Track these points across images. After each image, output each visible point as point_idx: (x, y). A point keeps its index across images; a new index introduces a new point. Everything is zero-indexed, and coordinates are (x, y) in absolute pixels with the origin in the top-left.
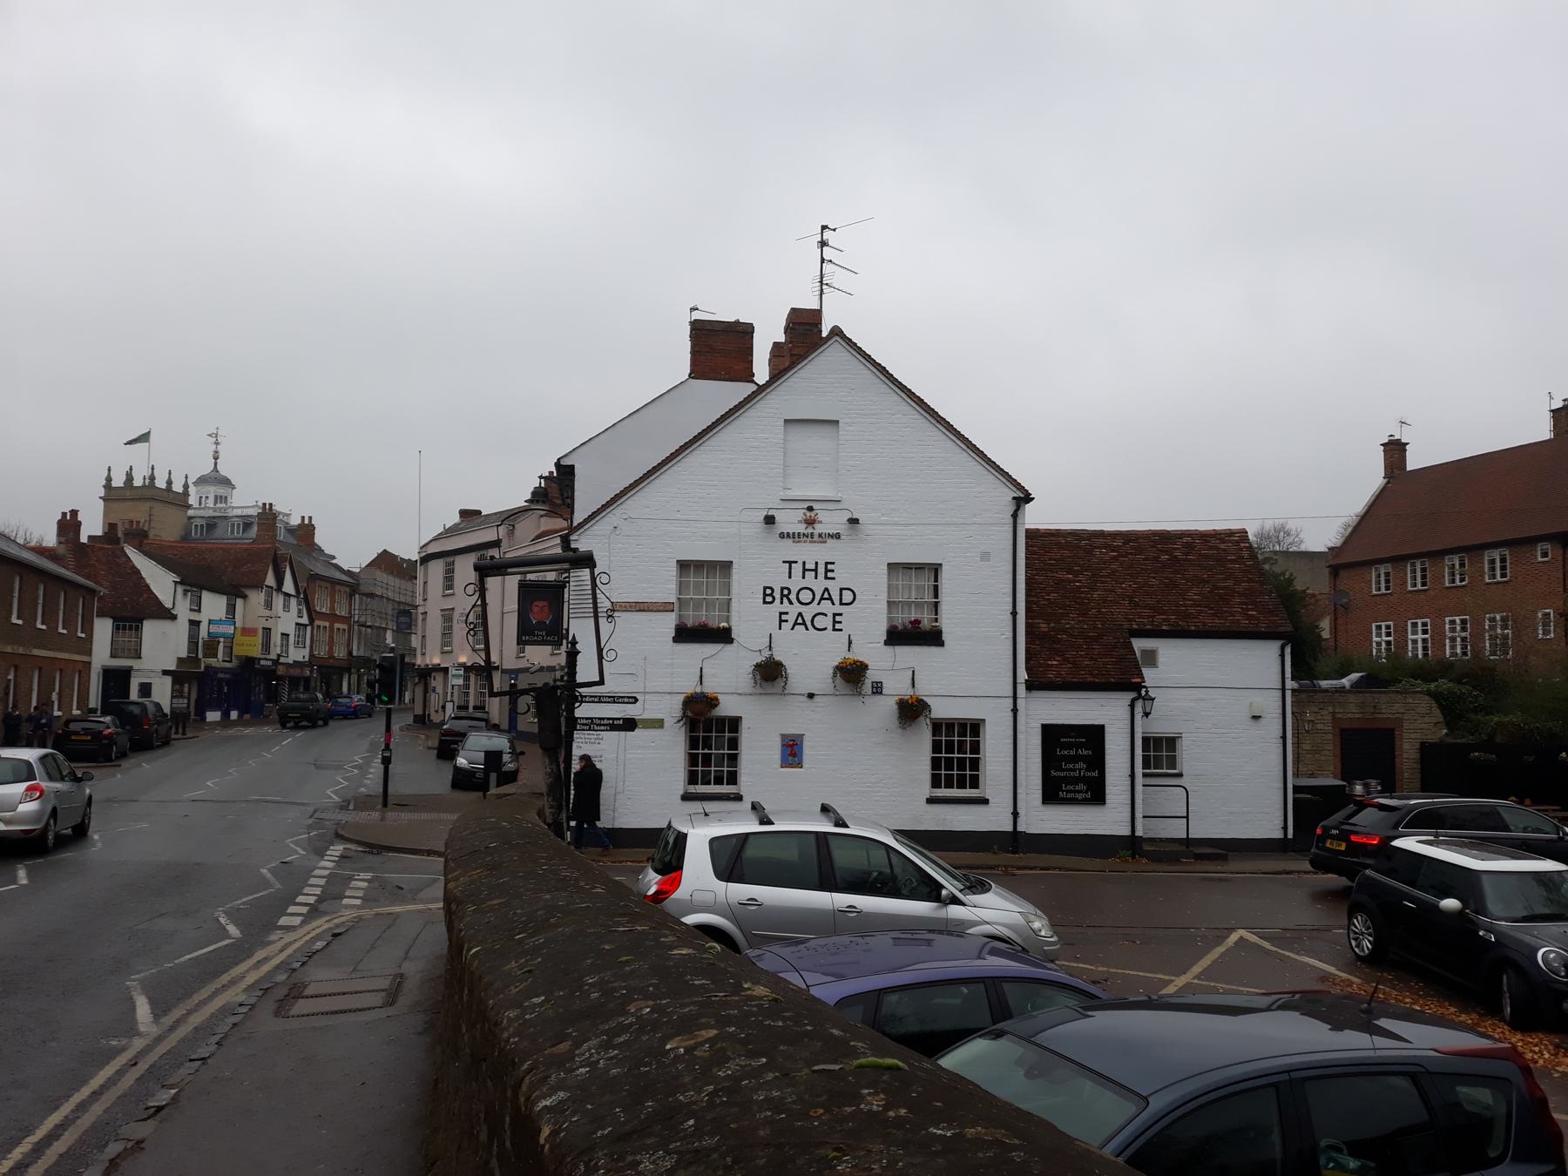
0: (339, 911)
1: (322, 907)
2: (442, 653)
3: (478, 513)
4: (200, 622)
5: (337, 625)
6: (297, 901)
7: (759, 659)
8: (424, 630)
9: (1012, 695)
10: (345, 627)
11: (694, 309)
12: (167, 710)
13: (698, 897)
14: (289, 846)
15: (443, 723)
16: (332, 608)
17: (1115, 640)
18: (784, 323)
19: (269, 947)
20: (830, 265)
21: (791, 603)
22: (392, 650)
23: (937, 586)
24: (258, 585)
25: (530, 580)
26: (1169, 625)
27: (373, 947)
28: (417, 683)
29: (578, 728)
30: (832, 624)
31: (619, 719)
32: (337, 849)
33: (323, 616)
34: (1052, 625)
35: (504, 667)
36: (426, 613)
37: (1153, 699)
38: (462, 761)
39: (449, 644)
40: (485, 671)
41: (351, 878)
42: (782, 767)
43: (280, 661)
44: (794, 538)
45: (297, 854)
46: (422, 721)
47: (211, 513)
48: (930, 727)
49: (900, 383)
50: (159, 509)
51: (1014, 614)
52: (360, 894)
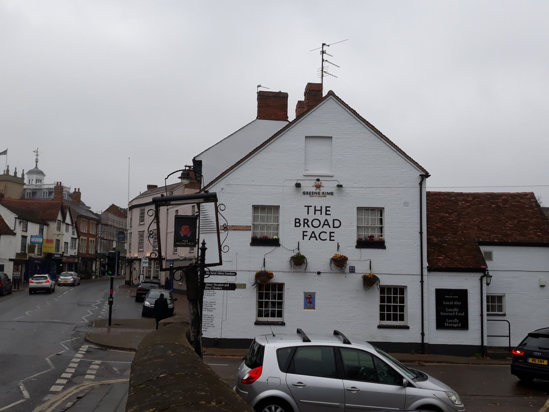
0: (83, 383)
1: (75, 380)
2: (139, 252)
3: (156, 186)
4: (27, 236)
5: (90, 239)
6: (62, 376)
7: (293, 254)
8: (130, 241)
9: (420, 274)
10: (94, 239)
11: (259, 86)
12: (10, 277)
13: (270, 381)
14: (61, 345)
15: (138, 285)
16: (88, 231)
17: (472, 247)
18: (304, 91)
19: (43, 404)
20: (327, 63)
21: (309, 226)
22: (114, 249)
23: (382, 218)
24: (54, 219)
25: (180, 215)
26: (498, 239)
27: (97, 407)
28: (127, 266)
29: (206, 288)
30: (329, 237)
31: (227, 284)
32: (85, 347)
33: (84, 234)
34: (439, 239)
35: (167, 259)
36: (131, 233)
37: (491, 277)
38: (147, 303)
39: (142, 247)
40: (160, 259)
41: (90, 363)
42: (304, 309)
43: (64, 255)
44: (310, 194)
45: (65, 349)
46: (129, 283)
47: (34, 187)
48: (379, 290)
49: (363, 118)
50: (10, 185)
51: (421, 233)
52: (94, 372)
